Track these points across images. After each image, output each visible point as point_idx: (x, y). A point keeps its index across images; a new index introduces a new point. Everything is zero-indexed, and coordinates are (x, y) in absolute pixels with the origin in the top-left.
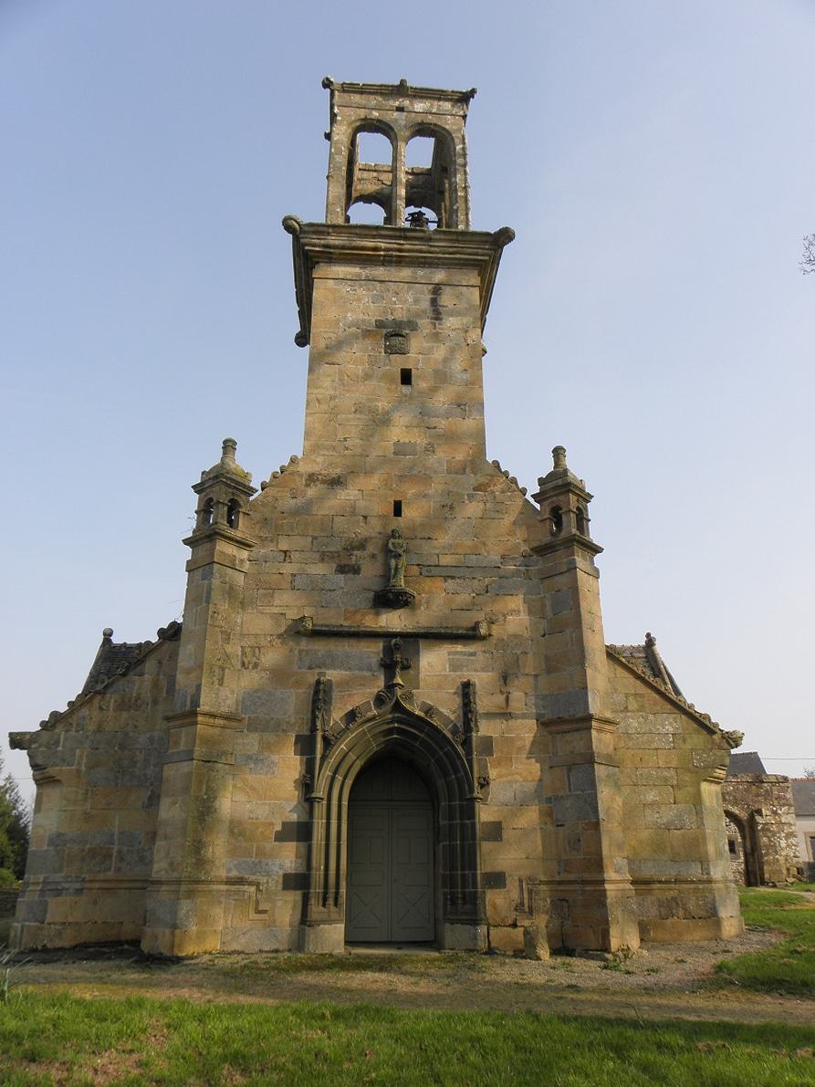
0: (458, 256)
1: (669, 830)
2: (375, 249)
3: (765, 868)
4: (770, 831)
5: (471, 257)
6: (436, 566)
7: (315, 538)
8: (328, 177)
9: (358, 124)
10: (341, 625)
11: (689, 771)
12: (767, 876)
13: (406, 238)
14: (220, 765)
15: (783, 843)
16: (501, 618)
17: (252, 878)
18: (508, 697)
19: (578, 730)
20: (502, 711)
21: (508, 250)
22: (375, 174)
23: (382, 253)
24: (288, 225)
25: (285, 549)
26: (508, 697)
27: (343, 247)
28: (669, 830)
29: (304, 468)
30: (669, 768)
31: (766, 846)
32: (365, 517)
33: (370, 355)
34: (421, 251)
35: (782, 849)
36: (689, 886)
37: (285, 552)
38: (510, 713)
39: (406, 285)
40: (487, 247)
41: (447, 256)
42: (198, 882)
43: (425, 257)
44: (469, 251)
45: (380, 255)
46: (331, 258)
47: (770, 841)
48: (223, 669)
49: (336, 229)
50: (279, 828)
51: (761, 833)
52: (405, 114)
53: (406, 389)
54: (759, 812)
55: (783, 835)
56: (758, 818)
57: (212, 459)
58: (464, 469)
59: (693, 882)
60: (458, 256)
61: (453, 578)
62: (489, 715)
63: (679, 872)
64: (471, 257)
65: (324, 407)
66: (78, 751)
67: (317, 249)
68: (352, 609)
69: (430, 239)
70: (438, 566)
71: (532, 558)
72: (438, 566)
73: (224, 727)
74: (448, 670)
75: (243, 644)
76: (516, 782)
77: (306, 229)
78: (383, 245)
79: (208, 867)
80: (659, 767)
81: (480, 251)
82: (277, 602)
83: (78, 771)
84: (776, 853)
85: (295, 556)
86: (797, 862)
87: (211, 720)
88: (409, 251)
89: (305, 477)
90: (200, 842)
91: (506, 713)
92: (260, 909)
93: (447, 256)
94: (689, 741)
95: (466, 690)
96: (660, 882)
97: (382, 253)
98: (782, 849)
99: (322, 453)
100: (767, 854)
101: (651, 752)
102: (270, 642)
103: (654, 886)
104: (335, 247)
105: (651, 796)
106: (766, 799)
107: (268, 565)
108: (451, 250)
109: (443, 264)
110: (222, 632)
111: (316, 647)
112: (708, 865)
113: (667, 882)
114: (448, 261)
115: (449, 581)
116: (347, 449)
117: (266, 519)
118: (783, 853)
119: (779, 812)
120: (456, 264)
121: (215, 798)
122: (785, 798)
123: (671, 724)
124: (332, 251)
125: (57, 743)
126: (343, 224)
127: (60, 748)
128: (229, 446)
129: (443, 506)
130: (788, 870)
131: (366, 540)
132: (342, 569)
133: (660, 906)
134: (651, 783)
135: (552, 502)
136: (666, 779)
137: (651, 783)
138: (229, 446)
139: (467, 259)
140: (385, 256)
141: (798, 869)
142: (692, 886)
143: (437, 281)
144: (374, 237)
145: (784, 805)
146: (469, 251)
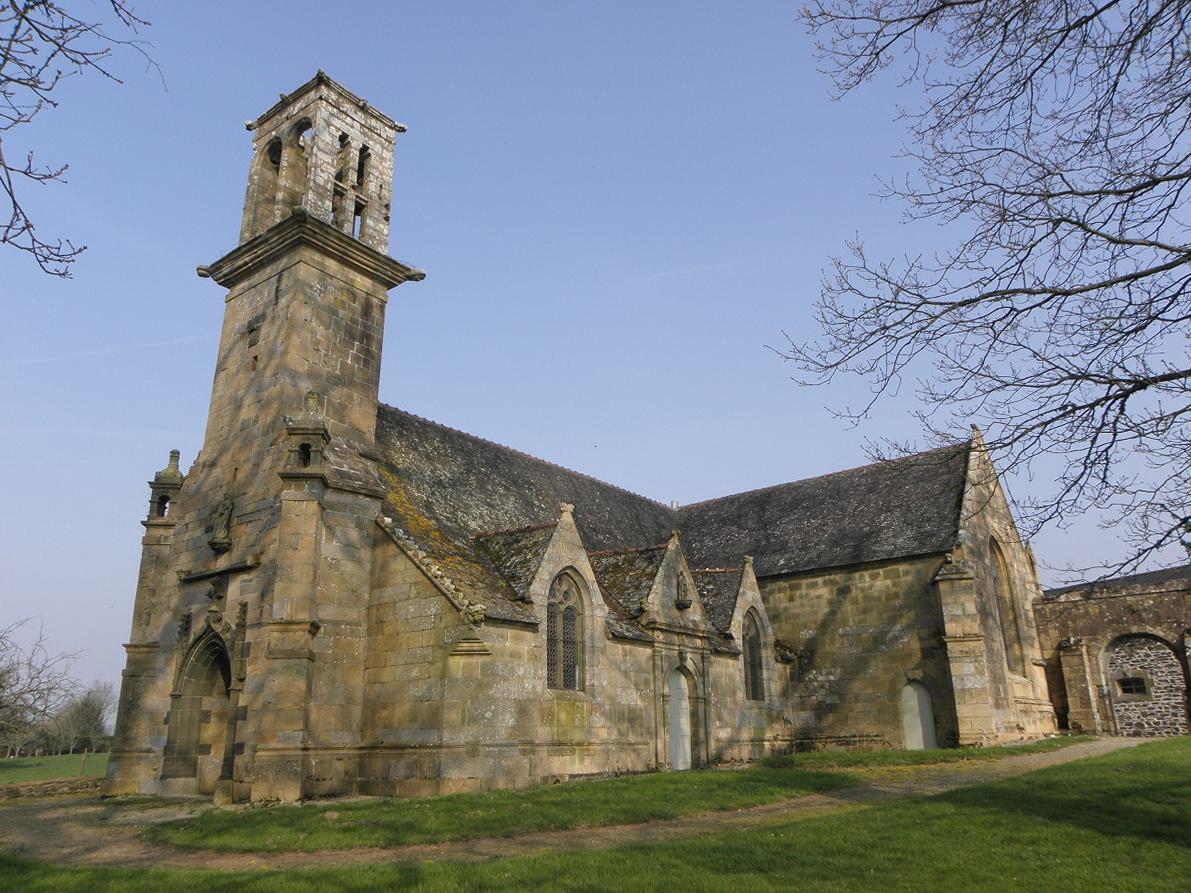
0: (286, 243)
2: (246, 264)
9: (267, 147)
11: (440, 647)
13: (256, 247)
21: (208, 264)
24: (205, 273)
34: (266, 251)
42: (123, 751)
44: (289, 235)
48: (149, 614)
57: (163, 464)
59: (429, 747)
60: (286, 243)
61: (250, 522)
69: (267, 240)
73: (148, 652)
78: (247, 259)
79: (132, 742)
84: (71, 838)
87: (137, 649)
88: (262, 254)
90: (126, 727)
94: (444, 620)
103: (407, 751)
104: (228, 274)
105: (415, 673)
108: (280, 241)
109: (283, 253)
113: (415, 747)
114: (284, 250)
121: (139, 699)
135: (163, 492)
136: (425, 657)
138: (175, 455)
139: (291, 243)
140: (253, 265)
142: (429, 751)
146: (289, 235)
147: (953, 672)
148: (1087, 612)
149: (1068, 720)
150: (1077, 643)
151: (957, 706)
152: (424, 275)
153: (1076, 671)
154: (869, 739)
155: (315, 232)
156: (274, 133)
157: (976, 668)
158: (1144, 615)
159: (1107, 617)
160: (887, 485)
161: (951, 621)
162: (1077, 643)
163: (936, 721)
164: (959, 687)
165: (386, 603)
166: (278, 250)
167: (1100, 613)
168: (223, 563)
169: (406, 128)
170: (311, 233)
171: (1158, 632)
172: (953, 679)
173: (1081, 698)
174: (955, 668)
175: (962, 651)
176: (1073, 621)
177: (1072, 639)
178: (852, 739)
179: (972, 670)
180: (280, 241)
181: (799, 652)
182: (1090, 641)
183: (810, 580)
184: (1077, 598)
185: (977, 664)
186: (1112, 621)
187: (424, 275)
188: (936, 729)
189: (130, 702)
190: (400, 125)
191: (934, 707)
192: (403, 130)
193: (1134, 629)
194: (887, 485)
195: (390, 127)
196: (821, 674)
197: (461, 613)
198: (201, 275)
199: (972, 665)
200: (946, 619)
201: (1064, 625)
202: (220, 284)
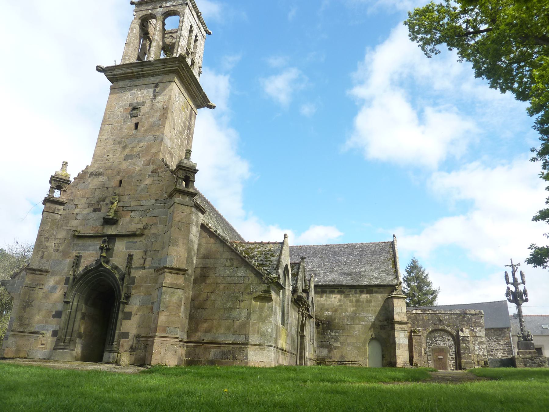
0: (165, 69)
1: (234, 320)
2: (132, 73)
3: (462, 360)
4: (467, 340)
5: (171, 69)
6: (129, 206)
7: (88, 198)
8: (125, 44)
10: (90, 233)
12: (463, 365)
14: (36, 289)
15: (477, 347)
16: (150, 226)
17: (42, 332)
18: (145, 260)
19: (174, 273)
20: (141, 266)
21: (104, 65)
22: (170, 34)
23: (135, 74)
25: (76, 204)
26: (145, 260)
27: (120, 74)
28: (234, 320)
29: (92, 170)
30: (239, 292)
31: (464, 348)
32: (107, 188)
33: (124, 119)
35: (476, 351)
36: (236, 346)
37: (76, 205)
38: (145, 267)
39: (145, 86)
40: (176, 63)
41: (161, 70)
43: (153, 72)
45: (135, 75)
46: (117, 80)
47: (467, 346)
49: (117, 67)
50: (54, 313)
51: (461, 342)
52: (162, 8)
53: (134, 132)
54: (462, 331)
55: (477, 343)
56: (461, 334)
58: (149, 164)
59: (239, 344)
60: (165, 69)
61: (135, 211)
62: (137, 268)
63: (235, 339)
64: (171, 69)
65: (102, 143)
66: (20, 286)
67: (111, 77)
68: (95, 226)
69: (153, 64)
70: (130, 206)
71: (167, 200)
72: (130, 206)
74: (124, 249)
75: (55, 242)
76: (141, 295)
77: (106, 69)
78: (134, 70)
80: (235, 292)
81: (174, 65)
82: (69, 225)
83: (20, 294)
85: (79, 206)
86: (485, 358)
89: (89, 173)
91: (143, 267)
92: (42, 343)
93: (161, 70)
95: (130, 256)
96: (225, 344)
97: (135, 74)
98: (476, 351)
99: (97, 163)
100: (464, 353)
101: (233, 285)
102: (64, 241)
104: (117, 75)
106: (467, 323)
107: (69, 210)
108: (162, 67)
110: (45, 238)
111: (79, 242)
112: (249, 337)
115: (133, 212)
116: (107, 160)
117: (72, 192)
118: (476, 353)
119: (475, 330)
120: (166, 73)
122: (479, 322)
123: (244, 272)
124: (116, 76)
125: (14, 284)
126: (135, 62)
127: (15, 286)
128: (65, 164)
129: (138, 180)
130: (478, 362)
131: (105, 198)
132: (95, 210)
133: (223, 354)
134: (230, 299)
137: (230, 299)
138: (65, 164)
141: (484, 361)
142: (239, 346)
143: (157, 82)
144: (131, 67)
145: (478, 326)
147: (396, 336)
148: (423, 318)
149: (413, 362)
150: (419, 330)
151: (397, 351)
152: (215, 107)
153: (418, 342)
154: (352, 363)
155: (183, 69)
156: (150, 11)
157: (405, 335)
158: (444, 322)
159: (431, 321)
160: (358, 254)
161: (397, 314)
162: (419, 330)
163: (383, 356)
164: (398, 343)
165: (209, 267)
166: (158, 72)
167: (428, 319)
168: (111, 231)
169: (211, 33)
170: (182, 69)
171: (449, 329)
172: (396, 339)
173: (419, 353)
174: (397, 334)
175: (400, 328)
176: (418, 322)
177: (417, 329)
178: (344, 363)
179: (403, 336)
180: (162, 67)
181: (323, 322)
182: (423, 330)
183: (331, 290)
184: (420, 312)
185: (405, 334)
186: (432, 323)
187: (215, 107)
188: (383, 360)
189: (27, 302)
190: (209, 31)
191: (383, 351)
192: (209, 33)
193: (440, 327)
194: (358, 254)
195: (205, 30)
196: (333, 332)
197: (263, 278)
198: (98, 70)
199: (403, 334)
200: (395, 313)
201: (414, 323)
202: (108, 78)
